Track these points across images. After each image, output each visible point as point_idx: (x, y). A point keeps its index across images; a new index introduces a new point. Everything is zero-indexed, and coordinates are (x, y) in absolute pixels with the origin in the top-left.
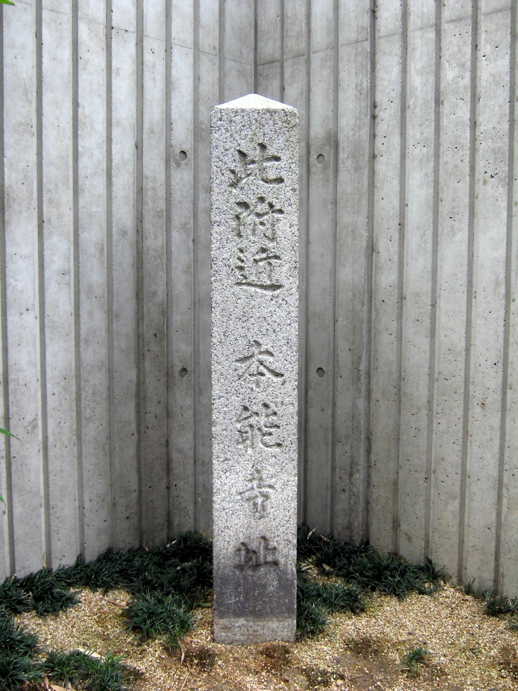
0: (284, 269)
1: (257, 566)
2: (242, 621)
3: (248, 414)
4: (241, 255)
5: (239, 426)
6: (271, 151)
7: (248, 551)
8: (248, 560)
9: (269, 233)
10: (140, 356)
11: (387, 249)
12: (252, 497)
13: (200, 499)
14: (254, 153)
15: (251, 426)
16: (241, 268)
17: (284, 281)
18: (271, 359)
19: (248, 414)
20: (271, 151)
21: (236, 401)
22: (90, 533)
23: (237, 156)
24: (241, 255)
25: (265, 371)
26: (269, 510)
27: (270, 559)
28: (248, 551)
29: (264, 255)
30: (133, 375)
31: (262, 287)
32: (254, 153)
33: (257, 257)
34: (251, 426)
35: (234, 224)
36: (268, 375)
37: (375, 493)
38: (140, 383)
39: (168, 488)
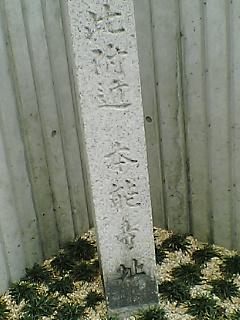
0: (132, 92)
1: (131, 276)
2: (126, 309)
3: (116, 188)
4: (100, 87)
5: (111, 197)
6: (113, 9)
7: (125, 268)
8: (124, 274)
9: (118, 69)
10: (23, 133)
11: (192, 37)
12: (124, 229)
13: (75, 211)
14: (100, 11)
15: (119, 196)
16: (102, 96)
17: (131, 101)
18: (128, 152)
19: (116, 188)
20: (113, 9)
21: (108, 182)
22: (11, 258)
23: (89, 16)
24: (100, 87)
25: (124, 160)
26: (136, 243)
27: (139, 271)
28: (125, 268)
29: (116, 85)
30: (20, 147)
31: (117, 106)
32: (100, 11)
33: (111, 87)
34: (119, 196)
35: (92, 66)
36: (127, 162)
37: (194, 197)
38: (26, 150)
39: (54, 210)
